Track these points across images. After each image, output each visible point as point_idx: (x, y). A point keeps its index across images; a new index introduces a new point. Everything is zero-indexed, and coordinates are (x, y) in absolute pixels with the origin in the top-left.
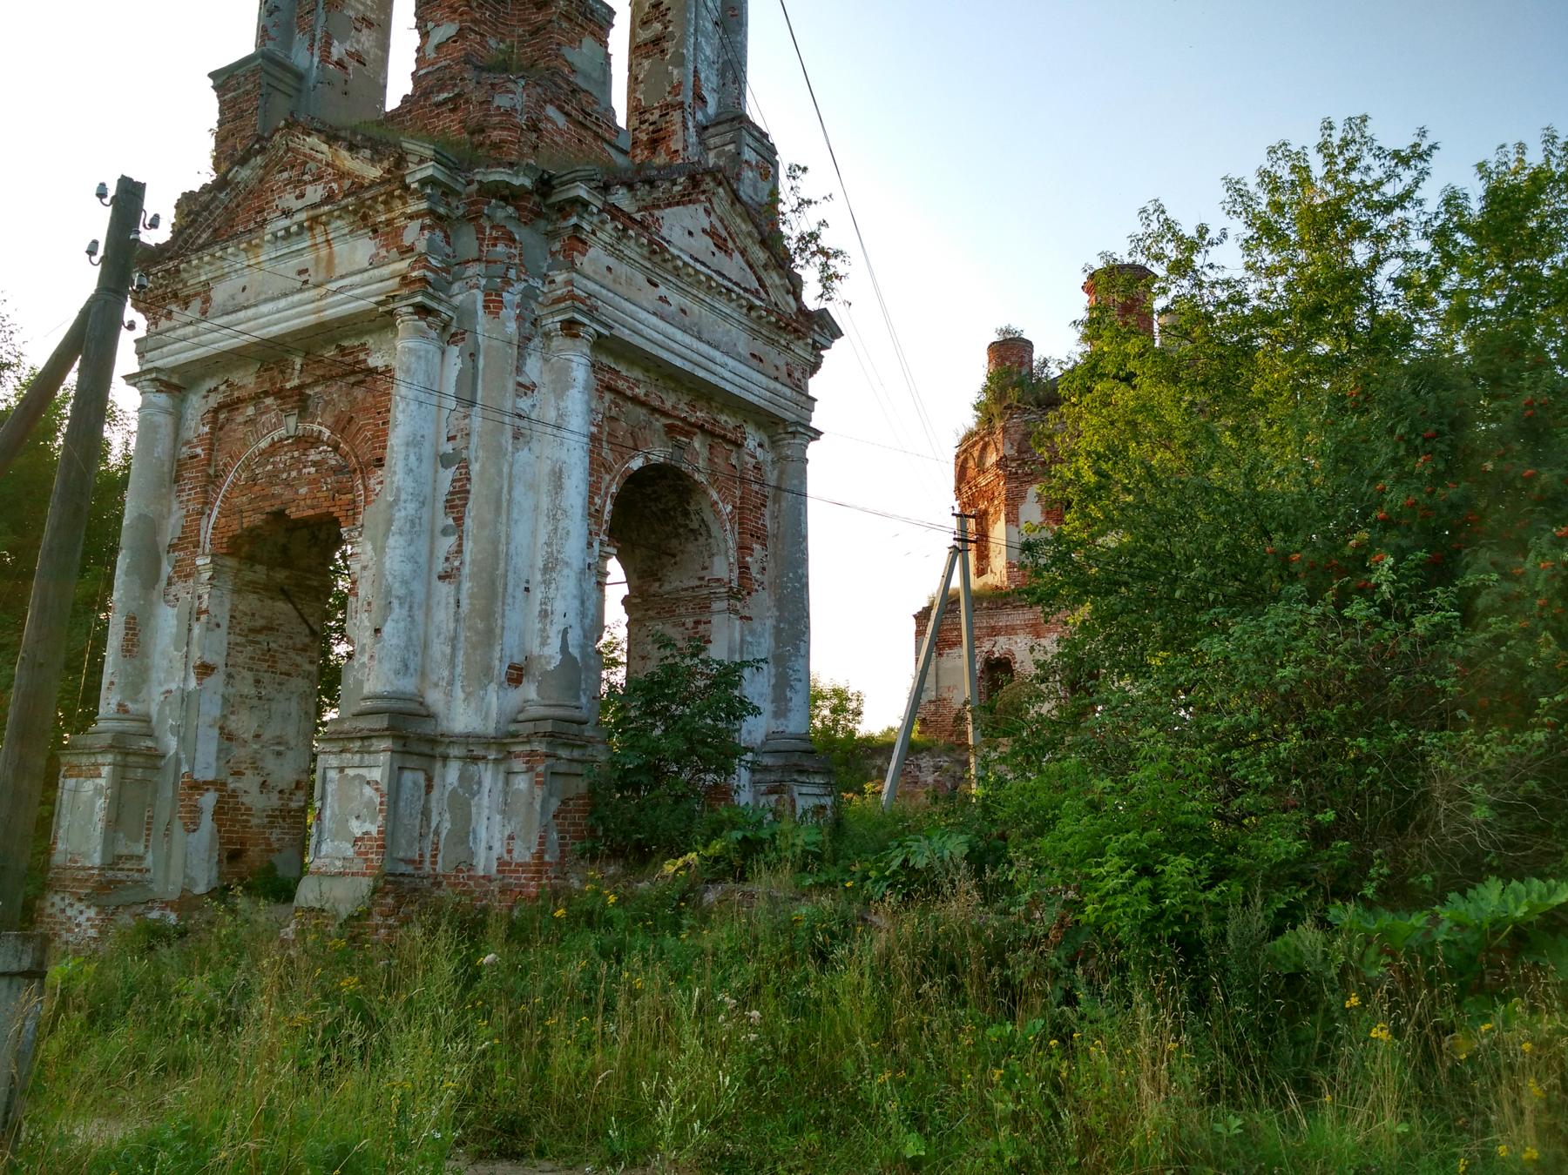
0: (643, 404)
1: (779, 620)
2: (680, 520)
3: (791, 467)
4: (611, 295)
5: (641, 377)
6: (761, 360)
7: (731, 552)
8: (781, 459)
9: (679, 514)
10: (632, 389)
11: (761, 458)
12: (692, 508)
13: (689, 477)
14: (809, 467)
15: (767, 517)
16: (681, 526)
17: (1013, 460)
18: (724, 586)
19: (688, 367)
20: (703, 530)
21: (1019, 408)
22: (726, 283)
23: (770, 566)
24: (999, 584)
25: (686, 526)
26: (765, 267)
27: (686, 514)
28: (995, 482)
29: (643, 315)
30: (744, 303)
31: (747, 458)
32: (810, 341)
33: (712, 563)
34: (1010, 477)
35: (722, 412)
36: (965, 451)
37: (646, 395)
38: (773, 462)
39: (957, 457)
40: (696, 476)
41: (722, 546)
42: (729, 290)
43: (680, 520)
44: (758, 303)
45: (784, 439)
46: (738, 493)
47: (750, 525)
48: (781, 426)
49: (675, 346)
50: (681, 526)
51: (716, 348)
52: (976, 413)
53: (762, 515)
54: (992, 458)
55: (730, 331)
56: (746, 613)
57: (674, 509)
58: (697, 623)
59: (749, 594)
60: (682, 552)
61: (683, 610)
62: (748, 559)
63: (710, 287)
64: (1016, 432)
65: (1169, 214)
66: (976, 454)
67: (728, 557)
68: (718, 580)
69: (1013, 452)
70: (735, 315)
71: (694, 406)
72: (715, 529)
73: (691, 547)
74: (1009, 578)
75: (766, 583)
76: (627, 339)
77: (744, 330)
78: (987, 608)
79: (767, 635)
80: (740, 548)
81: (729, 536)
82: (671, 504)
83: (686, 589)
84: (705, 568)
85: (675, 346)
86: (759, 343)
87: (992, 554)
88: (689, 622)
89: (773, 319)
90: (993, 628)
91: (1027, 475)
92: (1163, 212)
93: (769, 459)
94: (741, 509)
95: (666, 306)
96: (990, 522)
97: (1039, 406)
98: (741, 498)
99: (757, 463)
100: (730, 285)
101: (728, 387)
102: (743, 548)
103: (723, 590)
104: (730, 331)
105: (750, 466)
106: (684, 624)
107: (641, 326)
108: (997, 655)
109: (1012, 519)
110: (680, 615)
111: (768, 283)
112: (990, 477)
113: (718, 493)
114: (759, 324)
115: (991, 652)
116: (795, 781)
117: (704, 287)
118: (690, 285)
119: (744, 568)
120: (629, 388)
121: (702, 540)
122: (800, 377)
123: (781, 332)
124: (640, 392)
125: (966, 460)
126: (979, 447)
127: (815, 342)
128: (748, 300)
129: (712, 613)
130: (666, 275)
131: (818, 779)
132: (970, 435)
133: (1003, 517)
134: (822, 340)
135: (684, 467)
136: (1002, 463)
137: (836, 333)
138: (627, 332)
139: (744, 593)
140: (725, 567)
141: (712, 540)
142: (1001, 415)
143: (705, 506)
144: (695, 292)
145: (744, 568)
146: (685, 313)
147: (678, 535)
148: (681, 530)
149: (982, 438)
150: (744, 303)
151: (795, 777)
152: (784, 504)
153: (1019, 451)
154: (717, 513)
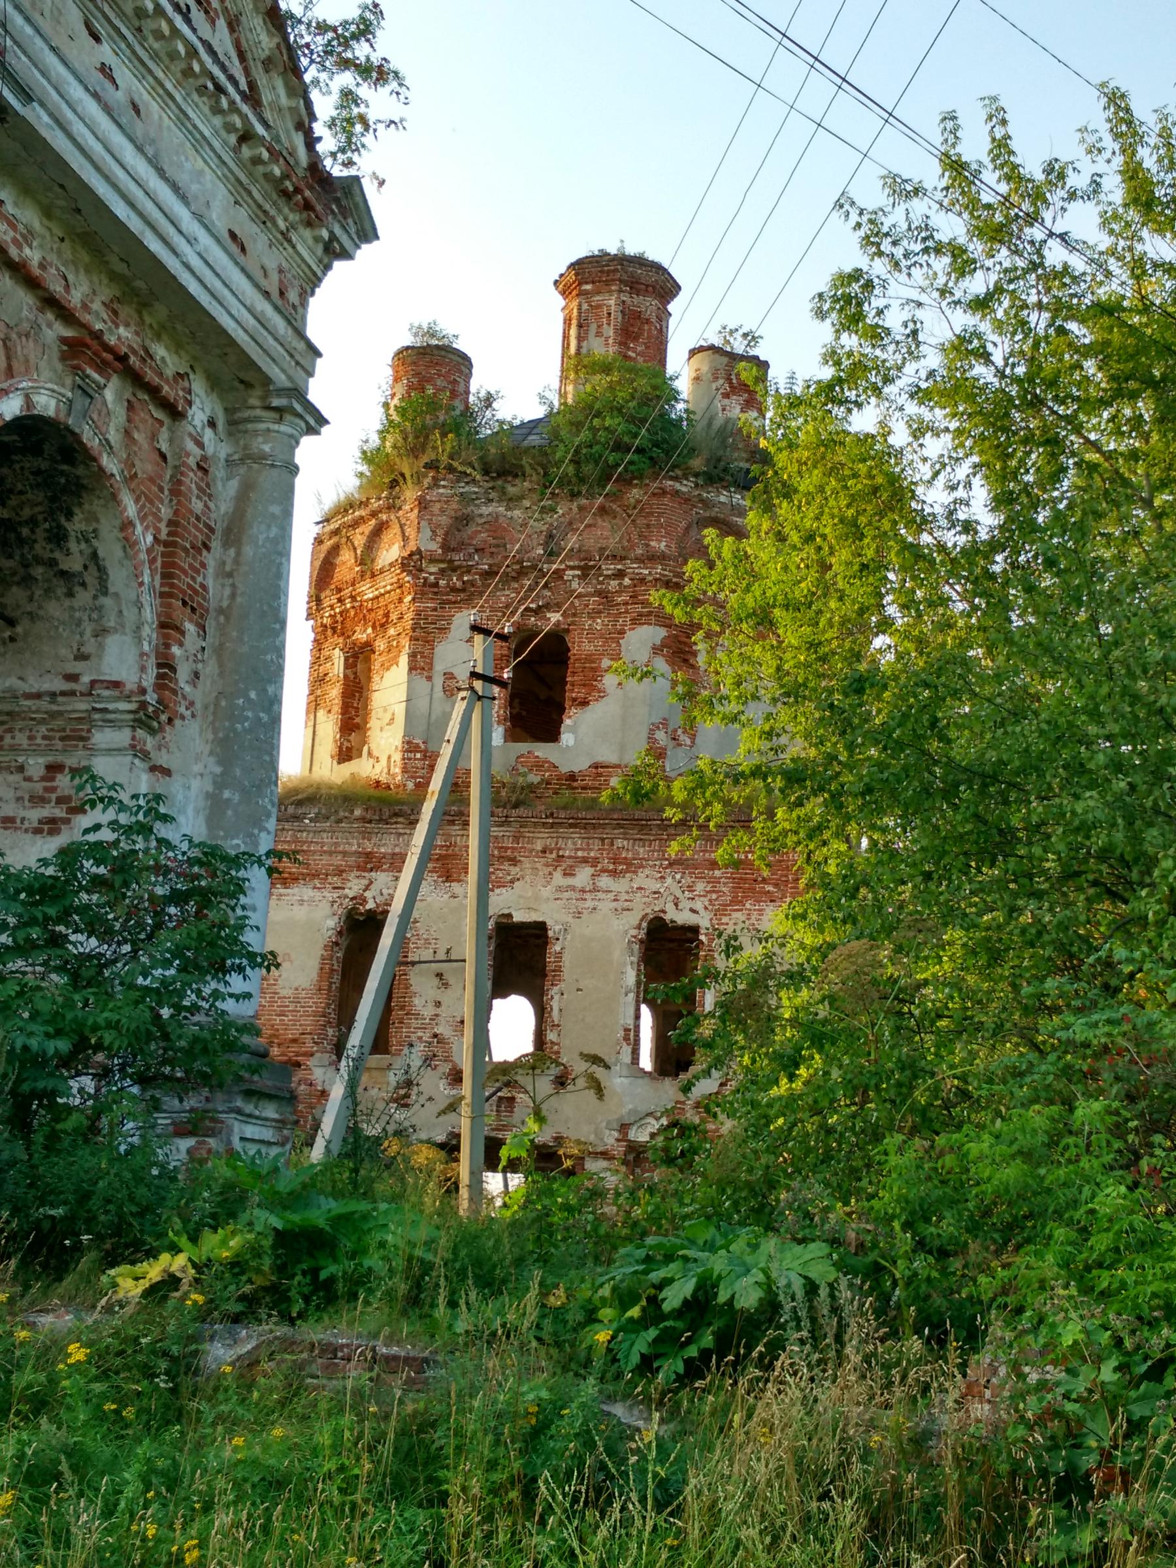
0: (32, 283)
1: (220, 783)
2: (41, 548)
3: (267, 478)
4: (29, 30)
5: (37, 225)
6: (243, 250)
7: (146, 631)
8: (250, 458)
9: (40, 534)
10: (20, 247)
11: (210, 450)
12: (76, 525)
13: (90, 458)
14: (299, 482)
15: (211, 570)
16: (39, 560)
17: (432, 561)
18: (128, 698)
19: (135, 224)
20: (90, 578)
21: (451, 469)
22: (216, 71)
23: (209, 669)
24: (383, 779)
25: (53, 563)
26: (268, 63)
27: (58, 537)
28: (394, 596)
29: (76, 92)
30: (238, 123)
31: (190, 446)
32: (325, 234)
33: (101, 646)
34: (425, 589)
35: (158, 337)
36: (336, 532)
37: (42, 266)
38: (229, 463)
39: (318, 541)
40: (105, 460)
41: (130, 615)
42: (219, 89)
43: (41, 548)
44: (260, 130)
45: (258, 420)
46: (165, 512)
47: (182, 582)
48: (258, 392)
49: (120, 174)
50: (39, 560)
51: (184, 198)
52: (364, 468)
53: (203, 565)
54: (390, 552)
55: (201, 173)
56: (162, 759)
57: (33, 522)
58: (53, 769)
59: (170, 720)
60: (32, 617)
61: (22, 739)
62: (175, 650)
63: (188, 72)
64: (442, 511)
65: (1011, 129)
66: (359, 540)
67: (139, 640)
68: (116, 685)
69: (434, 547)
70: (216, 144)
71: (115, 313)
72: (118, 577)
73: (54, 609)
74: (405, 770)
75: (198, 705)
76: (44, 133)
77: (224, 179)
78: (363, 819)
79: (190, 812)
80: (163, 625)
81: (146, 599)
82: (27, 512)
83: (38, 696)
84: (82, 657)
85: (120, 174)
86: (242, 213)
87: (374, 723)
88: (36, 765)
89: (277, 172)
90: (369, 856)
91: (454, 590)
92: (1004, 122)
93: (222, 455)
94: (168, 546)
95: (108, 85)
96: (376, 666)
97: (486, 472)
98: (170, 523)
99: (204, 458)
100: (222, 78)
101: (193, 288)
102: (168, 627)
103: (123, 706)
104: (201, 173)
105: (192, 462)
106: (21, 769)
107: (70, 115)
108: (370, 905)
109: (420, 665)
110: (14, 749)
111: (266, 97)
112: (386, 582)
113: (137, 501)
114: (250, 175)
115: (360, 899)
116: (239, 1111)
117: (181, 65)
118: (155, 56)
119: (166, 666)
120: (15, 241)
121: (83, 597)
122: (296, 301)
123: (281, 202)
124: (32, 255)
125: (336, 549)
126: (367, 528)
127: (333, 237)
128: (244, 118)
129: (92, 751)
130: (117, 22)
131: (270, 1111)
132: (346, 507)
133: (404, 660)
134: (344, 239)
135: (88, 436)
136: (411, 563)
137: (368, 233)
138: (46, 118)
139: (164, 718)
140: (131, 657)
141: (107, 601)
142: (418, 479)
143: (108, 529)
144: (160, 74)
145: (166, 666)
146: (137, 111)
147: (27, 581)
148: (38, 571)
149: (374, 514)
150: (238, 123)
151: (239, 1103)
152: (248, 551)
153: (445, 547)
154: (129, 544)
